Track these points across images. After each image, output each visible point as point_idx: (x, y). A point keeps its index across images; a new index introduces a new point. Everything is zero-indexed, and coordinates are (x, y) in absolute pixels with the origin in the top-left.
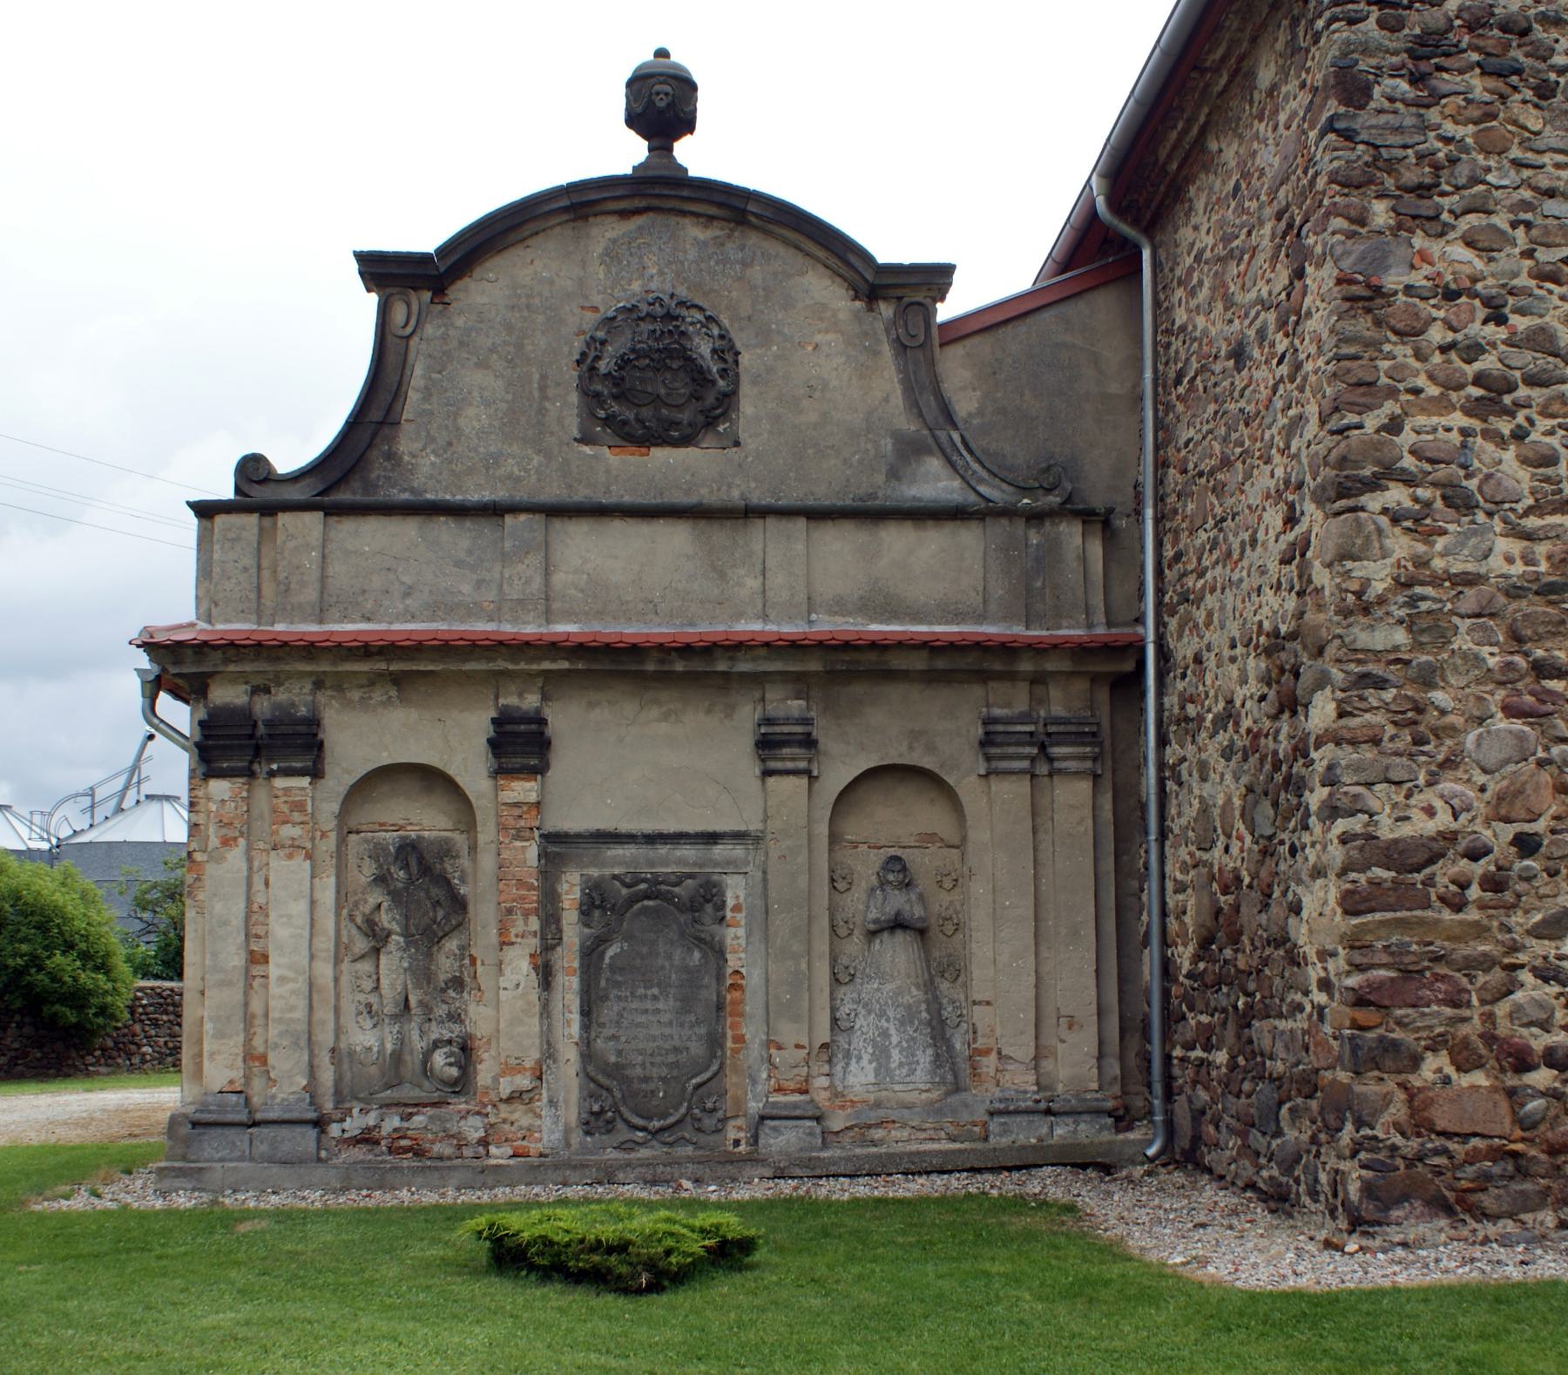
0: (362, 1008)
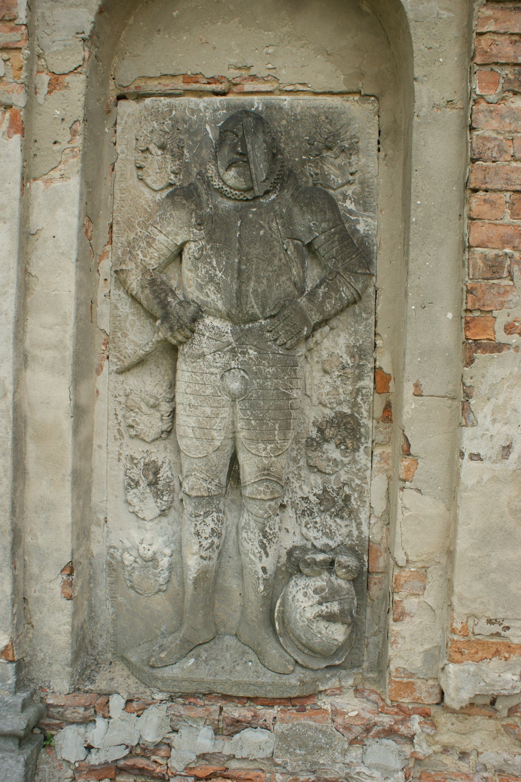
0: (136, 473)
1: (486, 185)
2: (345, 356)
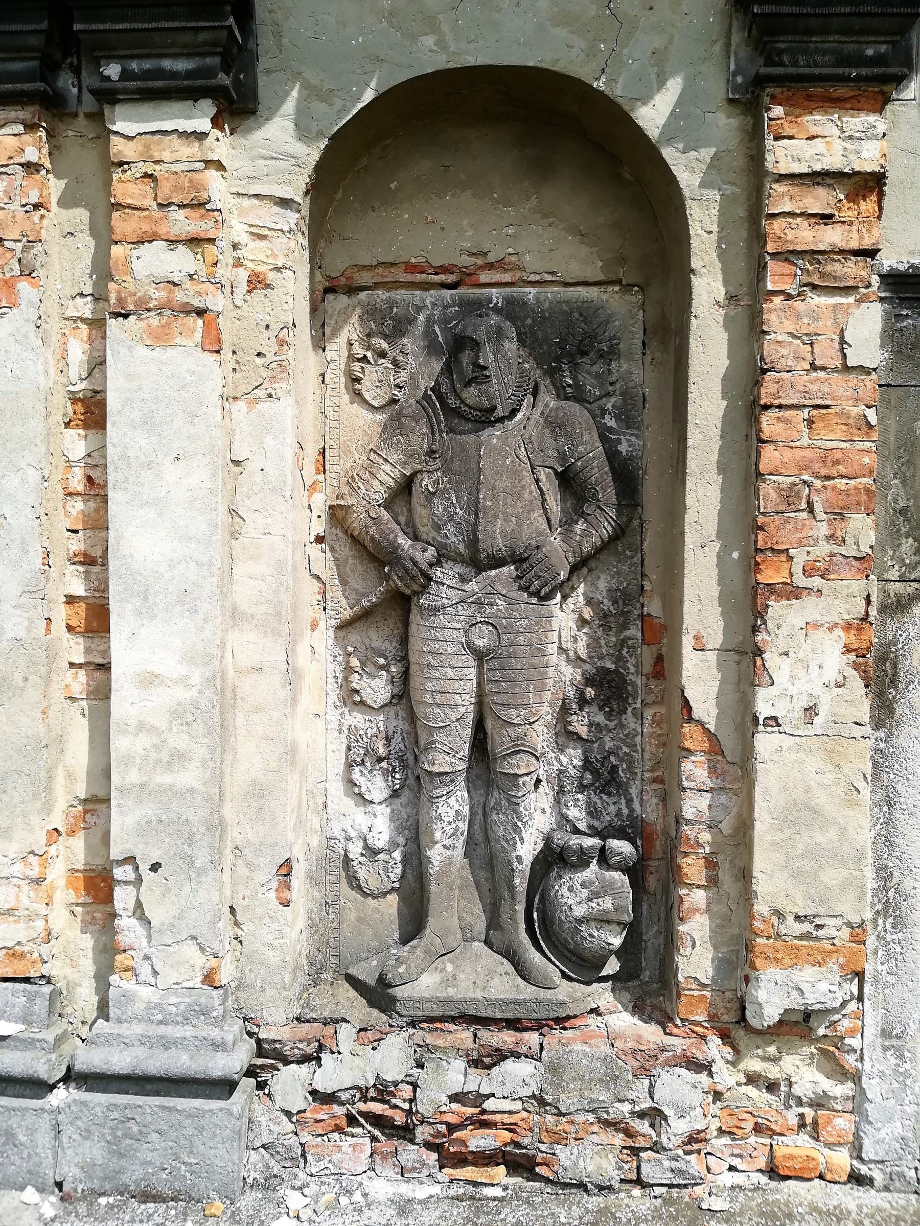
1: (780, 400)
2: (606, 601)
